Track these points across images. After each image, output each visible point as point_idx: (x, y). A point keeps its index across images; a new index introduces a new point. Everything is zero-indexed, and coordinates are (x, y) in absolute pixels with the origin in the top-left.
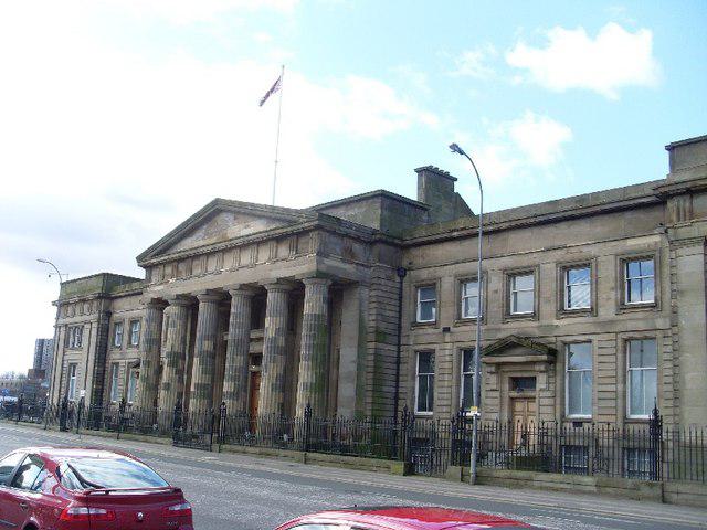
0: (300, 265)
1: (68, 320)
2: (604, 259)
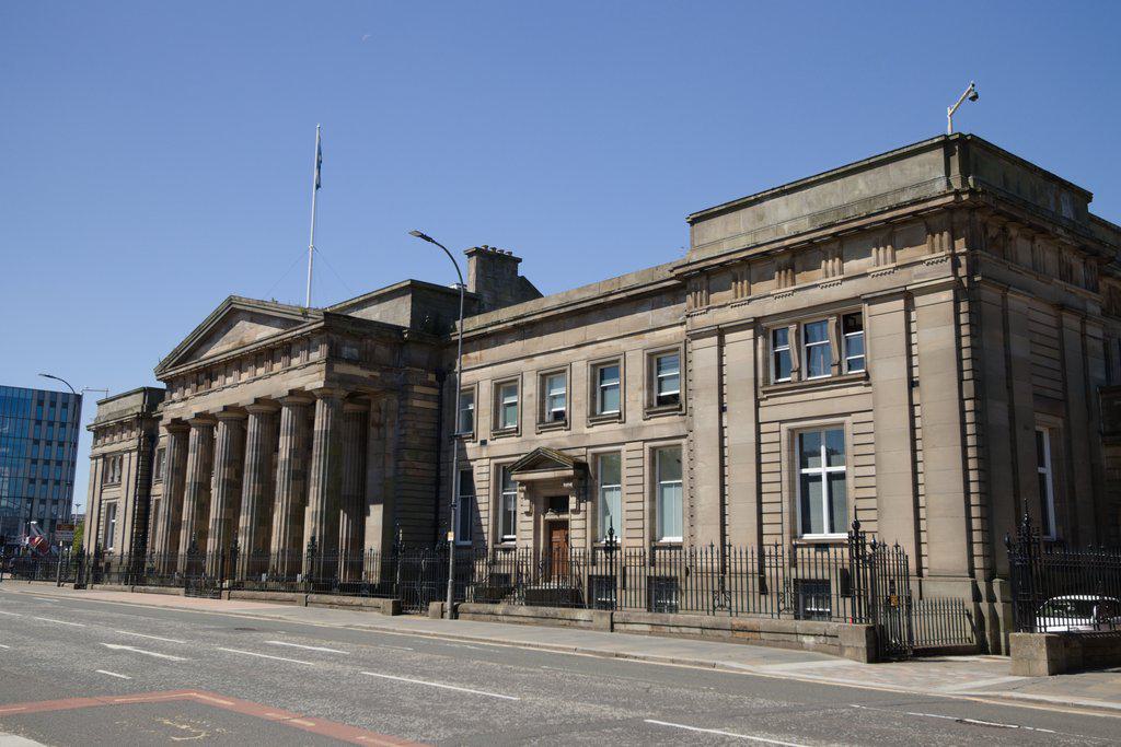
0: (307, 375)
1: (107, 449)
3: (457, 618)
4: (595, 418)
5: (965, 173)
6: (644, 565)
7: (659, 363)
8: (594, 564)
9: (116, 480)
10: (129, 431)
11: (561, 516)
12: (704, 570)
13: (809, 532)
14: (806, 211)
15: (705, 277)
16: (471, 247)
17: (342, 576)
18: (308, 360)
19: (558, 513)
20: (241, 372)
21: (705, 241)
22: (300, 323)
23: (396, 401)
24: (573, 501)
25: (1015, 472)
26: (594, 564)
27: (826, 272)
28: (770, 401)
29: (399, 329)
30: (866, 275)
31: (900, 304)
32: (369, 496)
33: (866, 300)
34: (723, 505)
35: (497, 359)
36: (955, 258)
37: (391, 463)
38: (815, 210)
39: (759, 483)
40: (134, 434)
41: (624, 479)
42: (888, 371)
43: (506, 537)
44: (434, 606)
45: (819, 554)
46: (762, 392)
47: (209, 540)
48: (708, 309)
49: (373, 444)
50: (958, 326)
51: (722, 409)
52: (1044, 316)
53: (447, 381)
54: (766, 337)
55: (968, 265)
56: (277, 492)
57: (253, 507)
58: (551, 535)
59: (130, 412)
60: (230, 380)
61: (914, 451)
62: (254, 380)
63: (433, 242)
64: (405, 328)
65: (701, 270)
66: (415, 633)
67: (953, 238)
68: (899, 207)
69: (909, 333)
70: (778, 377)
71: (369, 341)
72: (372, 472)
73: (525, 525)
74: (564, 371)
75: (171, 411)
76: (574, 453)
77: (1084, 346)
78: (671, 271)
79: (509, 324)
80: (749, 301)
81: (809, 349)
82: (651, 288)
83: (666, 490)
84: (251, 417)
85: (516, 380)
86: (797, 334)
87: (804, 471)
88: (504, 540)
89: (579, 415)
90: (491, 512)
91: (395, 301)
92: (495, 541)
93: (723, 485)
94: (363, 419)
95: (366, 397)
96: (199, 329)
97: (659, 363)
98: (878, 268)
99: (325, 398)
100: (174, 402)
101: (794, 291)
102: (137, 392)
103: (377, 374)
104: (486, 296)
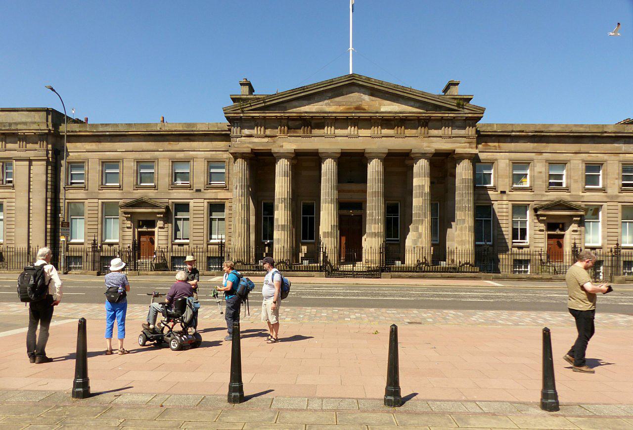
2: (611, 162)
11: (149, 230)
12: (24, 253)
16: (48, 85)
19: (148, 227)
35: (513, 150)
36: (47, 151)
63: (55, 92)
67: (47, 144)
70: (71, 180)
83: (73, 220)
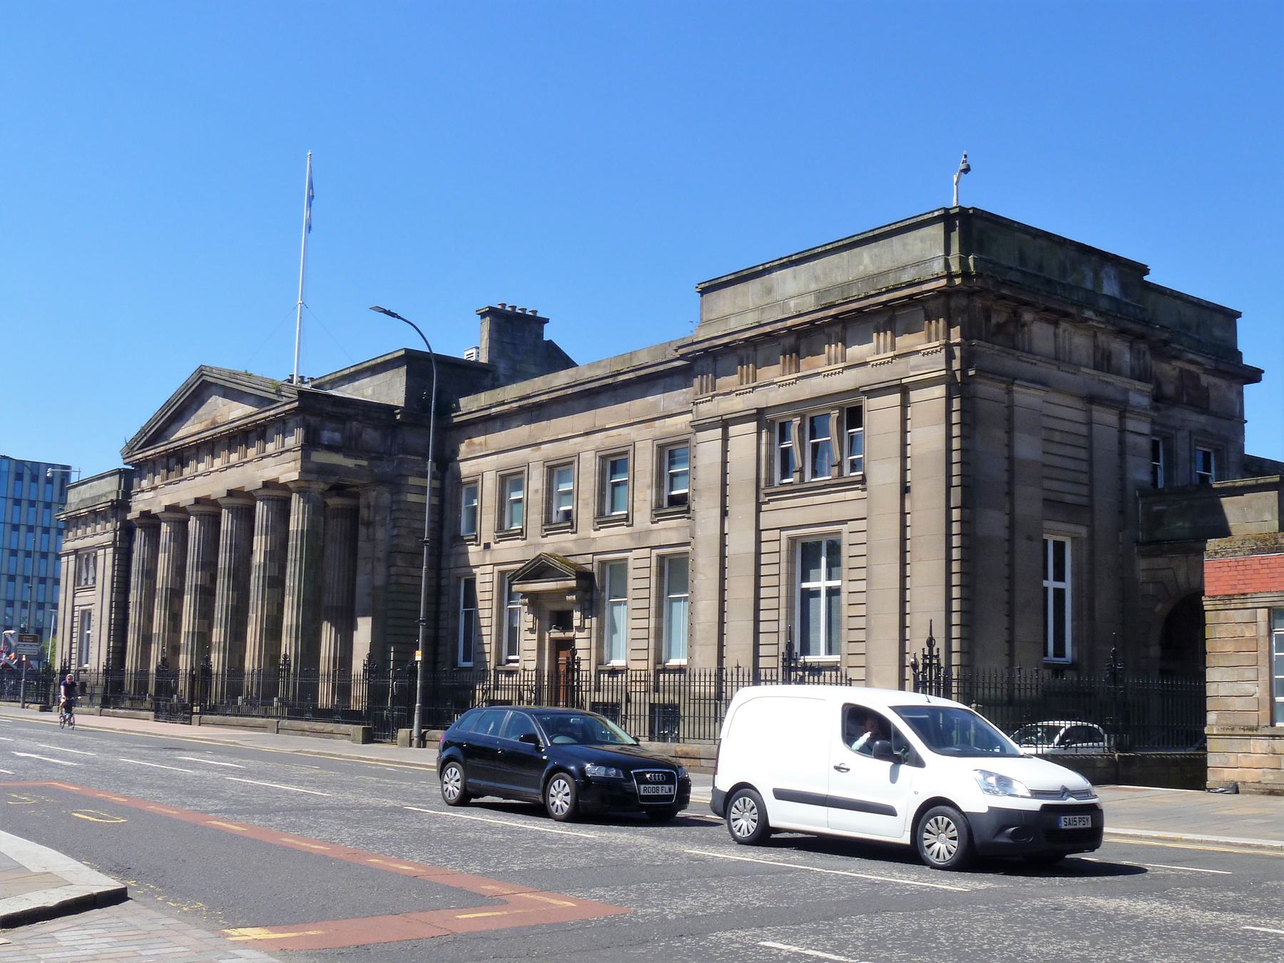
3: (424, 747)
4: (602, 519)
5: (965, 250)
6: (590, 691)
7: (671, 454)
8: (598, 689)
9: (90, 582)
10: (83, 527)
13: (809, 654)
14: (813, 287)
15: (752, 348)
16: (484, 306)
17: (325, 696)
18: (283, 446)
20: (213, 458)
21: (713, 316)
22: (275, 402)
23: (387, 495)
24: (577, 615)
25: (1011, 590)
26: (598, 689)
27: (829, 359)
28: (773, 505)
29: (390, 409)
30: (866, 364)
31: (896, 398)
32: (359, 605)
33: (864, 393)
34: (721, 623)
35: (503, 446)
36: (949, 348)
37: (381, 569)
38: (822, 285)
39: (757, 598)
40: (108, 525)
41: (630, 591)
42: (883, 474)
43: (511, 658)
44: (403, 733)
45: (507, 679)
46: (763, 494)
47: (181, 656)
48: (713, 397)
49: (363, 545)
50: (949, 425)
51: (724, 513)
52: (1067, 411)
53: (450, 470)
54: (770, 431)
55: (962, 357)
56: (251, 601)
57: (226, 618)
58: (558, 656)
59: (104, 499)
60: (202, 467)
61: (903, 564)
62: (227, 468)
63: (399, 317)
64: (397, 407)
65: (705, 350)
66: (360, 758)
67: (950, 325)
68: (503, 403)
69: (904, 432)
71: (354, 423)
72: (361, 580)
73: (528, 643)
74: (571, 463)
75: (142, 502)
76: (580, 560)
77: (1122, 443)
78: (676, 350)
79: (515, 405)
80: (754, 388)
81: (815, 446)
82: (661, 368)
84: (224, 512)
85: (521, 472)
86: (801, 428)
87: (805, 585)
88: (509, 661)
89: (586, 515)
90: (494, 628)
91: (389, 374)
92: (499, 663)
93: (722, 601)
94: (352, 515)
95: (355, 489)
96: (168, 404)
97: (671, 454)
98: (742, 387)
99: (302, 492)
100: (142, 491)
101: (797, 379)
102: (112, 474)
103: (364, 463)
104: (502, 367)
